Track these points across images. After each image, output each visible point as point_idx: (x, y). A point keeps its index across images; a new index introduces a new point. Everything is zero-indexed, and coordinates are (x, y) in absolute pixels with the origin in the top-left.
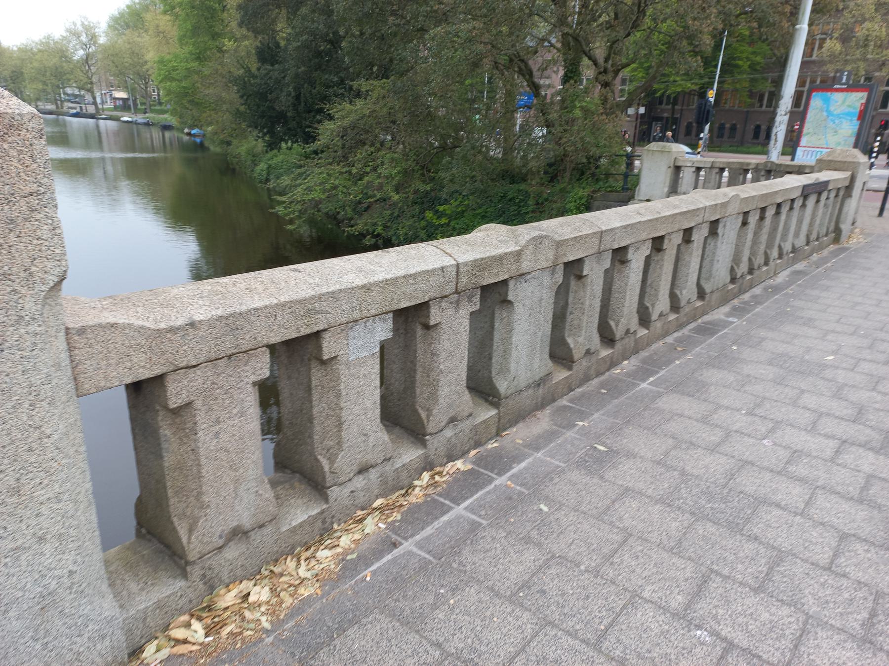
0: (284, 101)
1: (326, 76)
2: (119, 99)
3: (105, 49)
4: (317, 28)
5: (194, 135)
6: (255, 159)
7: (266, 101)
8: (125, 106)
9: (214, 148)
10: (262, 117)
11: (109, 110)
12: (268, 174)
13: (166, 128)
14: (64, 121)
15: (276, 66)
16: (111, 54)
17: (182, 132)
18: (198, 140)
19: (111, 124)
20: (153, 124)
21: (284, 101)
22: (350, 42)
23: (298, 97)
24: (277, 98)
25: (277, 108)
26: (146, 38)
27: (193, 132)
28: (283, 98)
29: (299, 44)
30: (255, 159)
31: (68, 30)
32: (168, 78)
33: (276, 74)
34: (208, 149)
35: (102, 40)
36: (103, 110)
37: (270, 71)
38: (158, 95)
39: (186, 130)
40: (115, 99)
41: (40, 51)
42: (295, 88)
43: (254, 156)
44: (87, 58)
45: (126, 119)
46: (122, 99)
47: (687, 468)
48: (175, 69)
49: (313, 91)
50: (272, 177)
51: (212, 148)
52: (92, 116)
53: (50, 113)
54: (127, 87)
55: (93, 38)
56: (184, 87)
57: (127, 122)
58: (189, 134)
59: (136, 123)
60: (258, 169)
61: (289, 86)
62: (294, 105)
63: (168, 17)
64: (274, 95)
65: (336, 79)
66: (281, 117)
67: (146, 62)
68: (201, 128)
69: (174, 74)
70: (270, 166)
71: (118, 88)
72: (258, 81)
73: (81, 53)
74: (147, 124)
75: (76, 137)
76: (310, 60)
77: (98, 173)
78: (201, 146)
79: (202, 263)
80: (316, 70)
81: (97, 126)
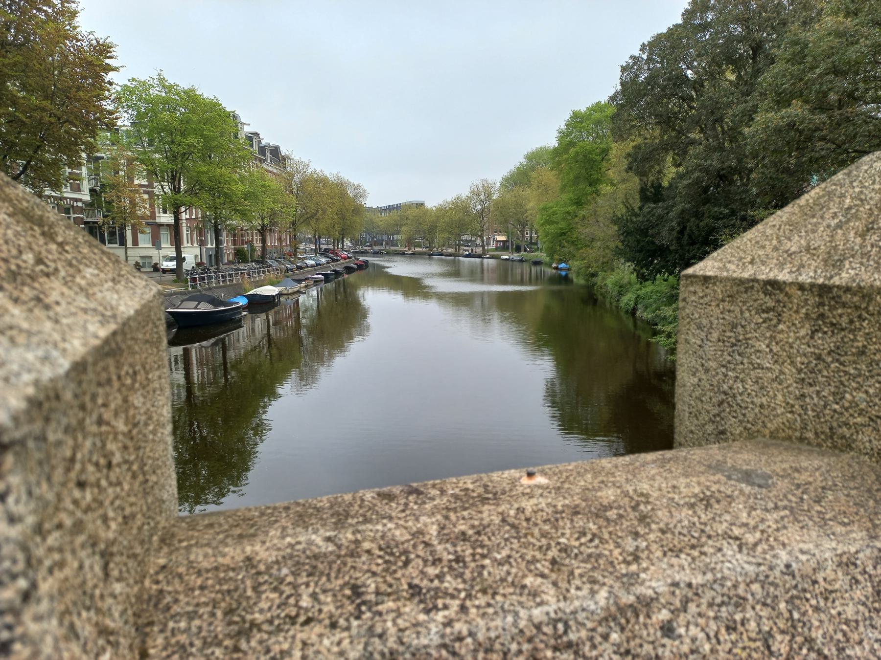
0: (665, 236)
1: (716, 209)
2: (500, 241)
3: (496, 202)
4: (711, 165)
5: (561, 269)
6: (622, 289)
7: (646, 237)
8: (504, 246)
9: (579, 281)
10: (640, 251)
11: (492, 250)
12: (636, 304)
13: (537, 263)
14: (459, 260)
15: (660, 204)
16: (501, 207)
17: (550, 266)
18: (563, 273)
19: (492, 262)
20: (526, 261)
21: (665, 236)
22: (763, 173)
23: (681, 232)
24: (659, 233)
25: (657, 242)
26: (528, 191)
27: (560, 266)
28: (665, 232)
29: (690, 181)
30: (622, 289)
31: (471, 192)
32: (549, 222)
33: (660, 211)
34: (572, 281)
35: (495, 197)
36: (488, 250)
37: (653, 209)
38: (531, 236)
39: (554, 265)
40: (497, 241)
41: (450, 209)
42: (679, 224)
43: (620, 287)
44: (481, 213)
45: (505, 257)
46: (503, 241)
47: (117, 559)
48: (554, 213)
49: (701, 224)
50: (639, 306)
51: (575, 280)
52: (479, 256)
53: (450, 255)
54: (508, 232)
55: (489, 195)
56: (561, 229)
57: (506, 259)
58: (556, 268)
59: (513, 261)
60: (625, 299)
61: (672, 221)
62: (678, 239)
63: (554, 172)
64: (655, 231)
65: (727, 211)
66: (662, 251)
67: (526, 211)
68: (565, 262)
69: (554, 218)
70: (638, 296)
71: (501, 233)
72: (640, 219)
73: (479, 207)
74: (521, 261)
75: (464, 270)
76: (700, 195)
77: (478, 302)
78: (566, 280)
79: (557, 382)
80: (704, 204)
81: (482, 264)
